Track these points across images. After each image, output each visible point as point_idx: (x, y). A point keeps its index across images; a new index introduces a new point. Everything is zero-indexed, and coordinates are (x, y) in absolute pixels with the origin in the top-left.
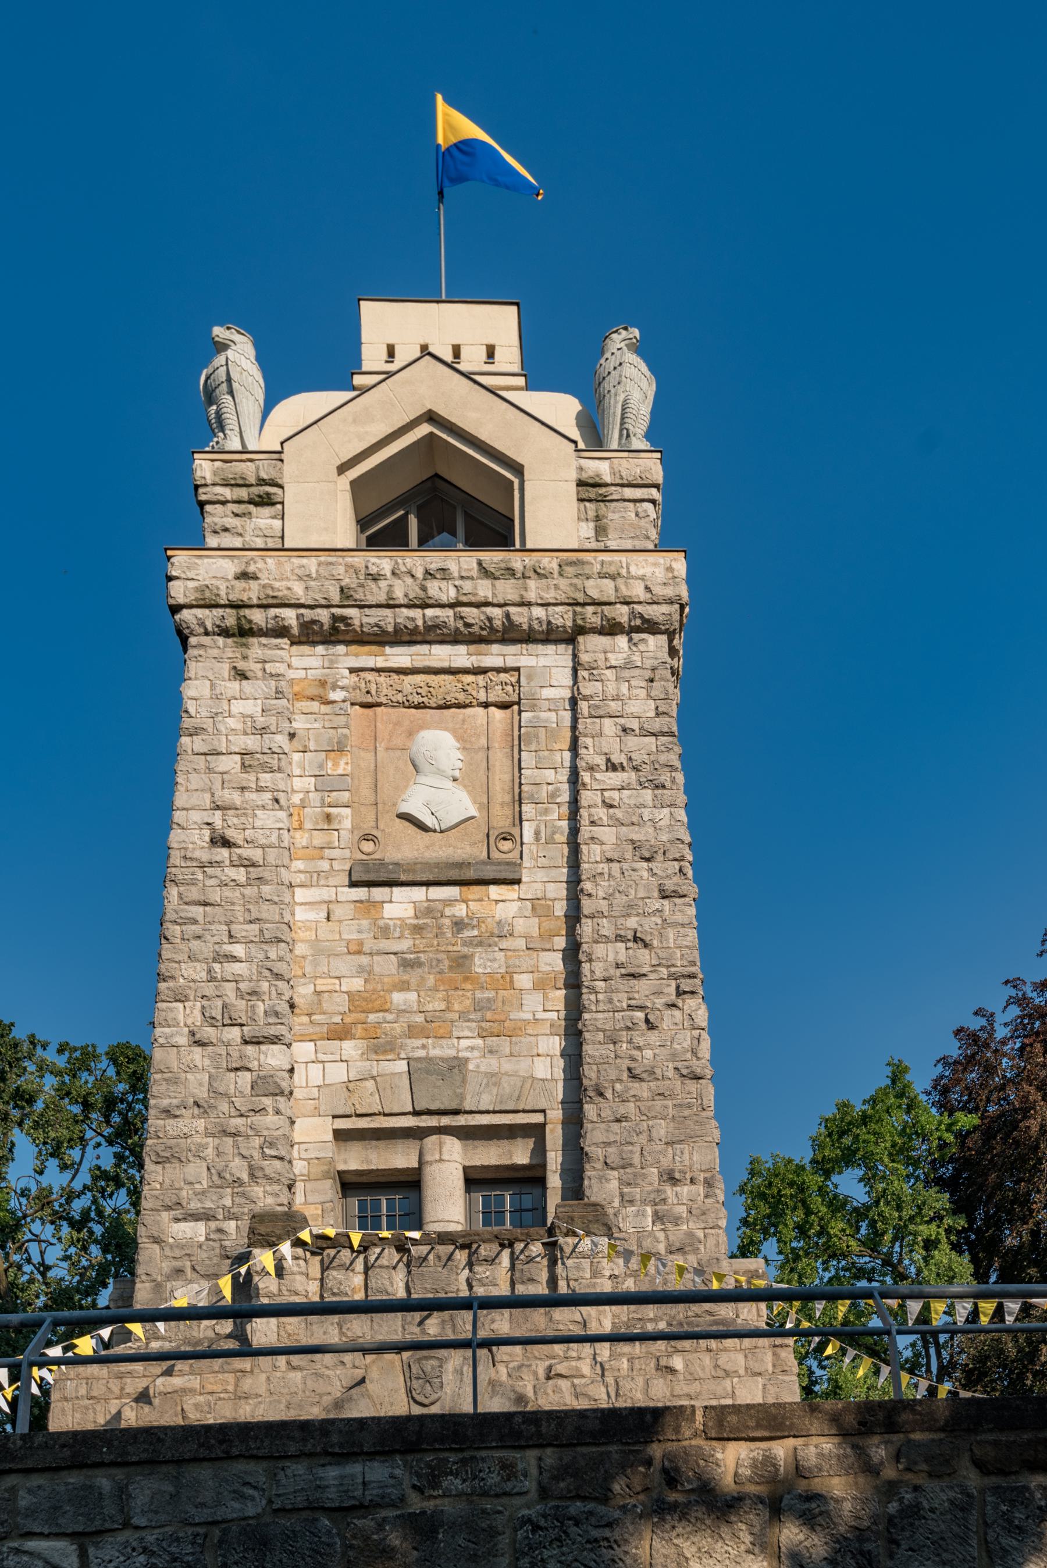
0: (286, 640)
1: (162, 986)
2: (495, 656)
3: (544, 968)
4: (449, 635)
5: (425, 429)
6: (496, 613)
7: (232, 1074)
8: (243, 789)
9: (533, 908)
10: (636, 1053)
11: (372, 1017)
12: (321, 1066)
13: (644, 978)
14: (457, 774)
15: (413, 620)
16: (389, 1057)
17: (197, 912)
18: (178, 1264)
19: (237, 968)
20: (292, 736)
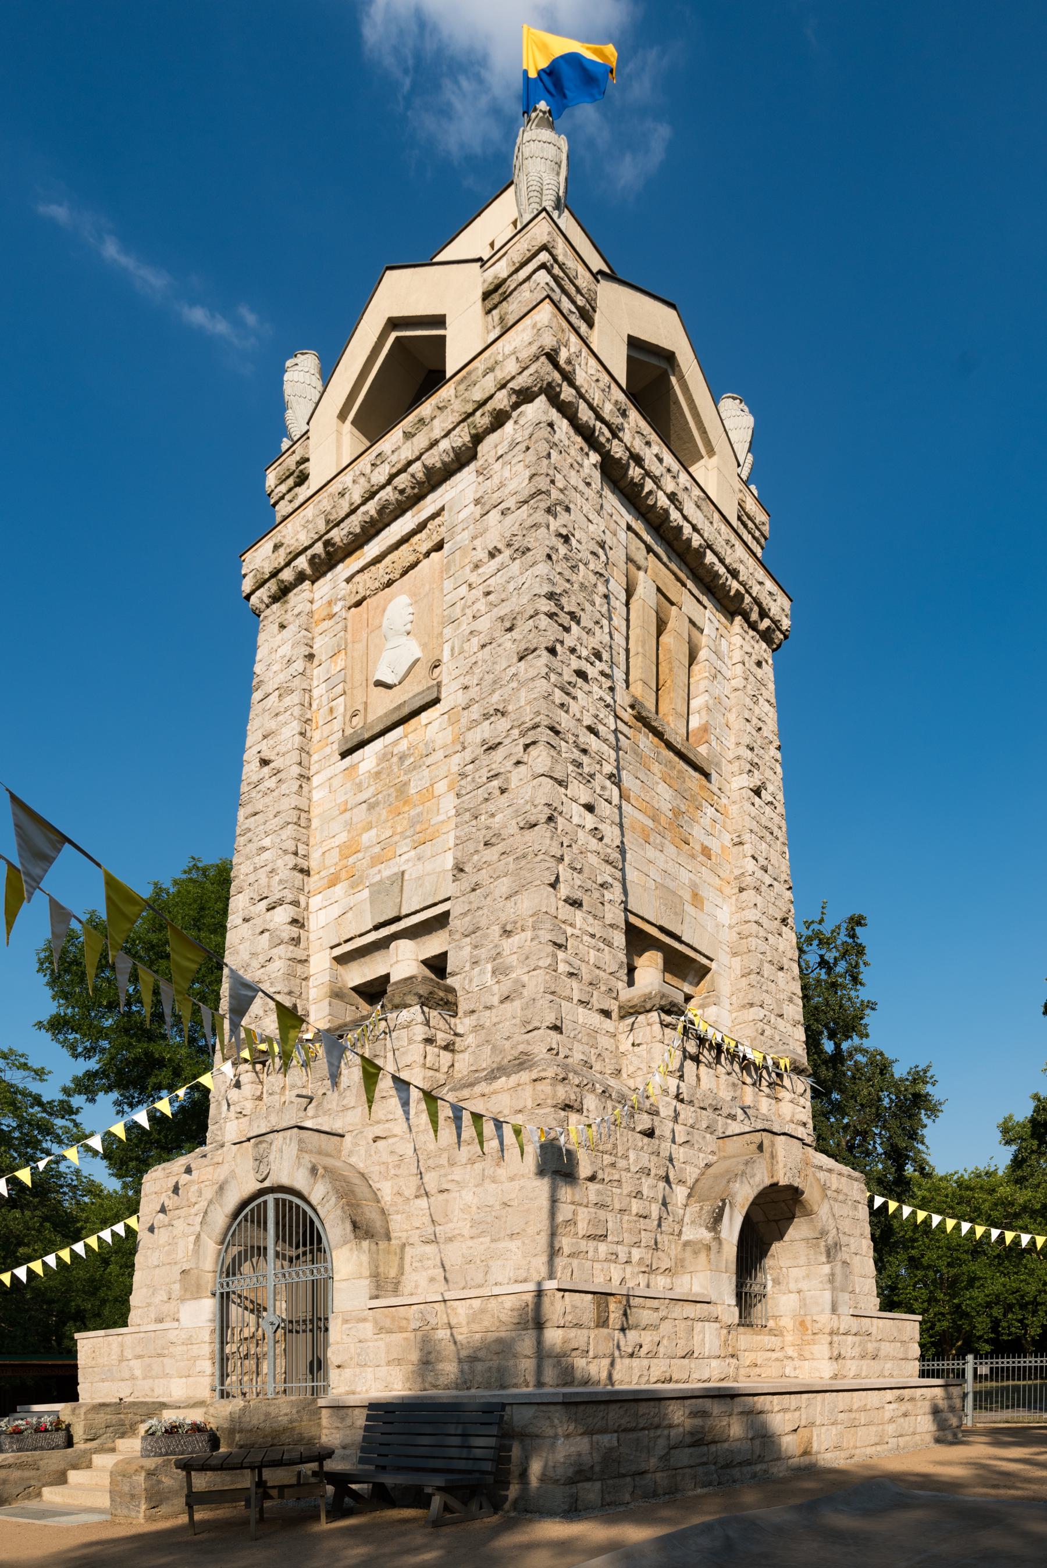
0: (307, 582)
4: (395, 509)
6: (418, 465)
13: (500, 746)
14: (409, 627)
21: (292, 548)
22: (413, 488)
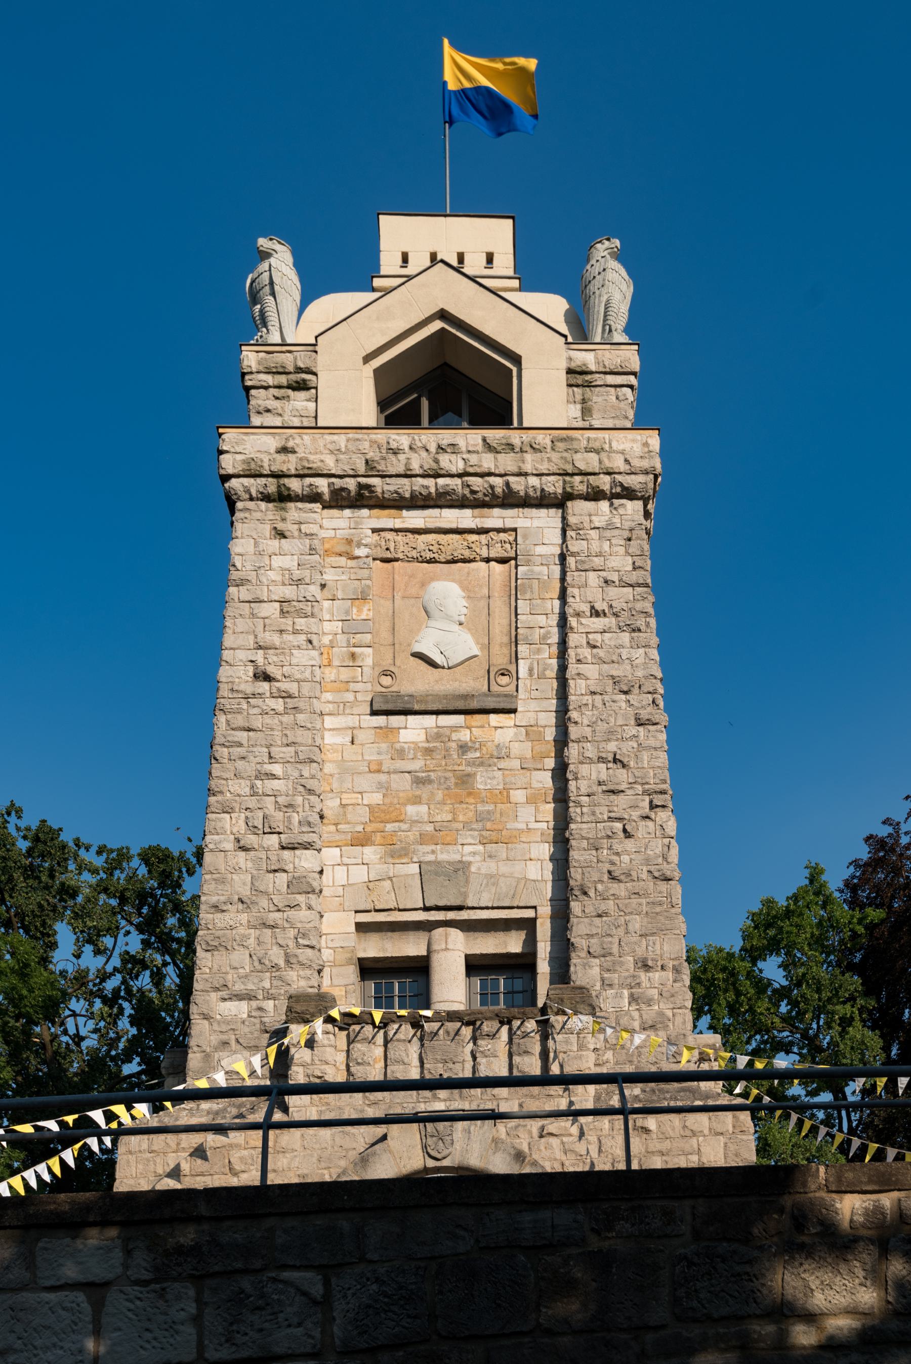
0: (318, 505)
1: (212, 799)
3: (535, 785)
4: (458, 500)
5: (437, 325)
7: (271, 875)
9: (527, 734)
10: (615, 858)
11: (389, 827)
12: (345, 868)
14: (463, 619)
15: (427, 487)
17: (242, 736)
18: (224, 1037)
19: (275, 784)
20: (323, 586)
21: (314, 466)
22: (485, 495)
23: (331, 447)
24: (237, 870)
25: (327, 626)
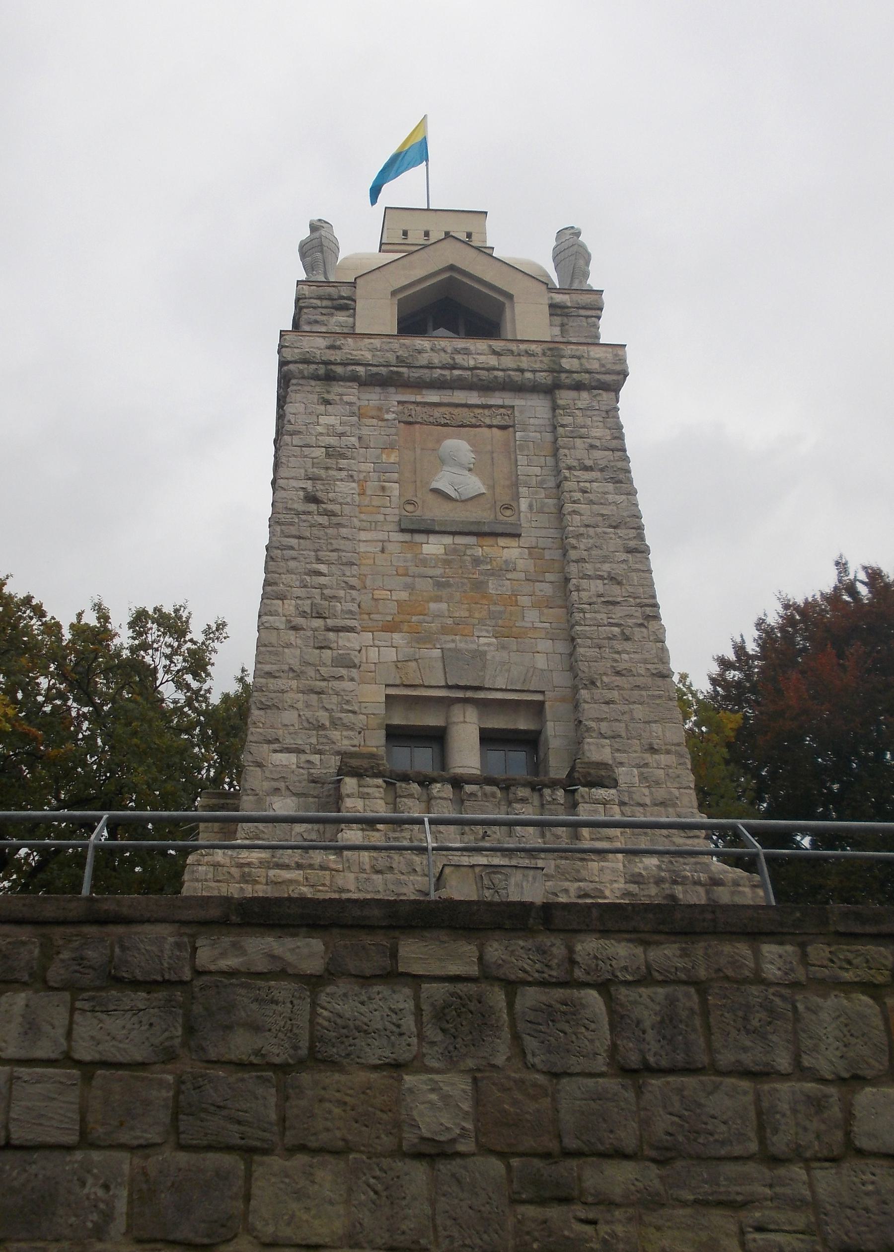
2: (496, 399)
3: (538, 593)
7: (318, 651)
8: (327, 468)
9: (530, 554)
10: (617, 656)
11: (414, 618)
12: (377, 649)
14: (472, 466)
15: (444, 375)
16: (427, 646)
17: (294, 542)
18: (275, 784)
19: (322, 580)
20: (360, 438)
23: (370, 347)
24: (289, 645)
25: (363, 467)
